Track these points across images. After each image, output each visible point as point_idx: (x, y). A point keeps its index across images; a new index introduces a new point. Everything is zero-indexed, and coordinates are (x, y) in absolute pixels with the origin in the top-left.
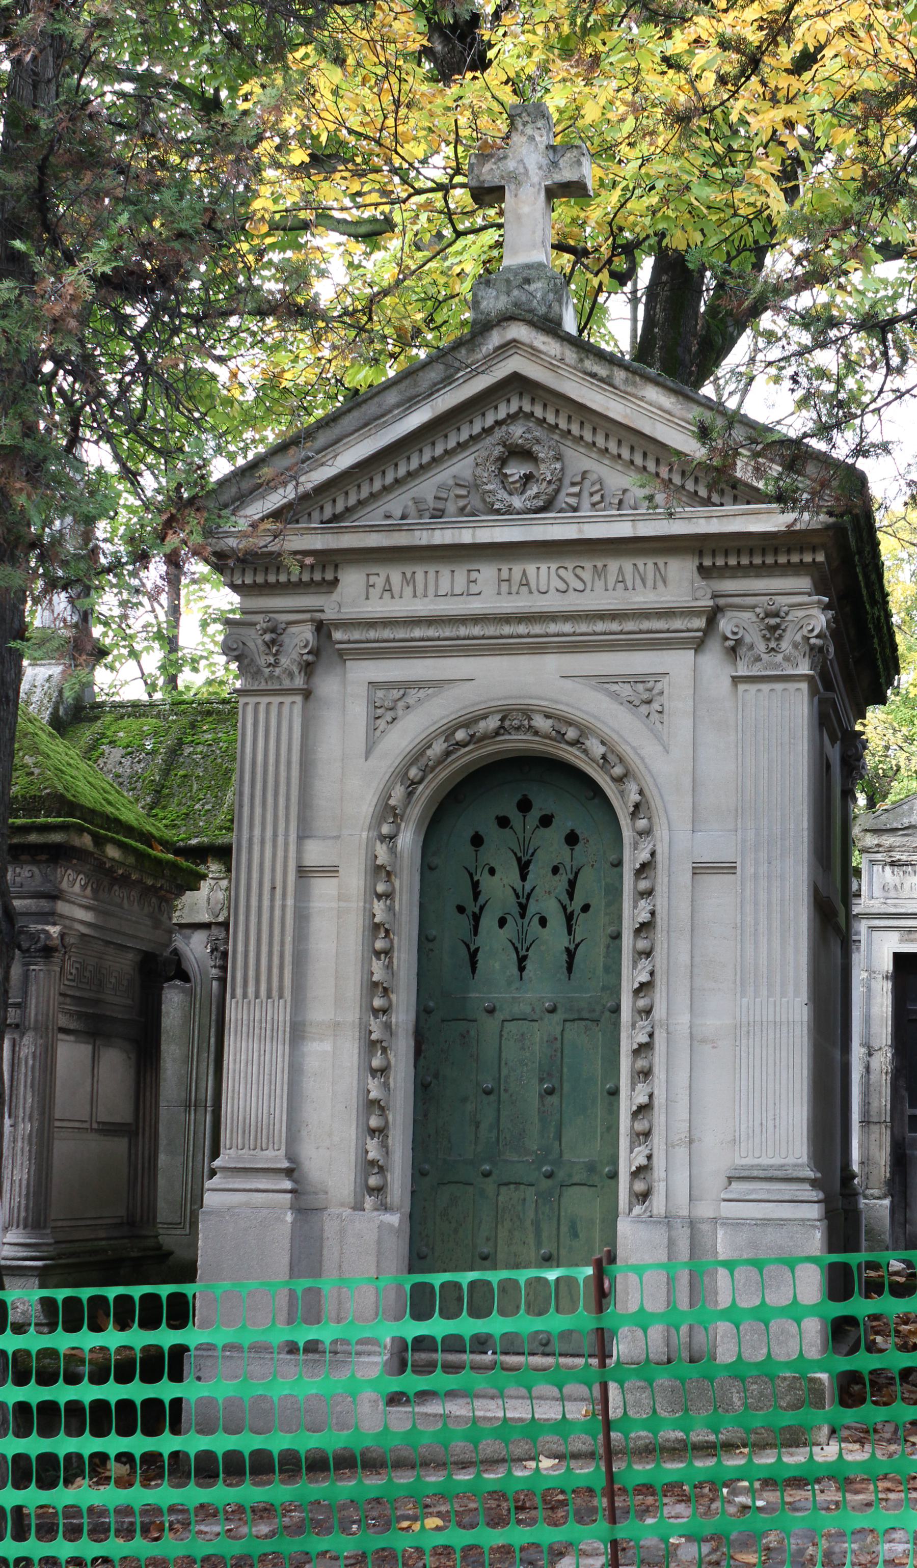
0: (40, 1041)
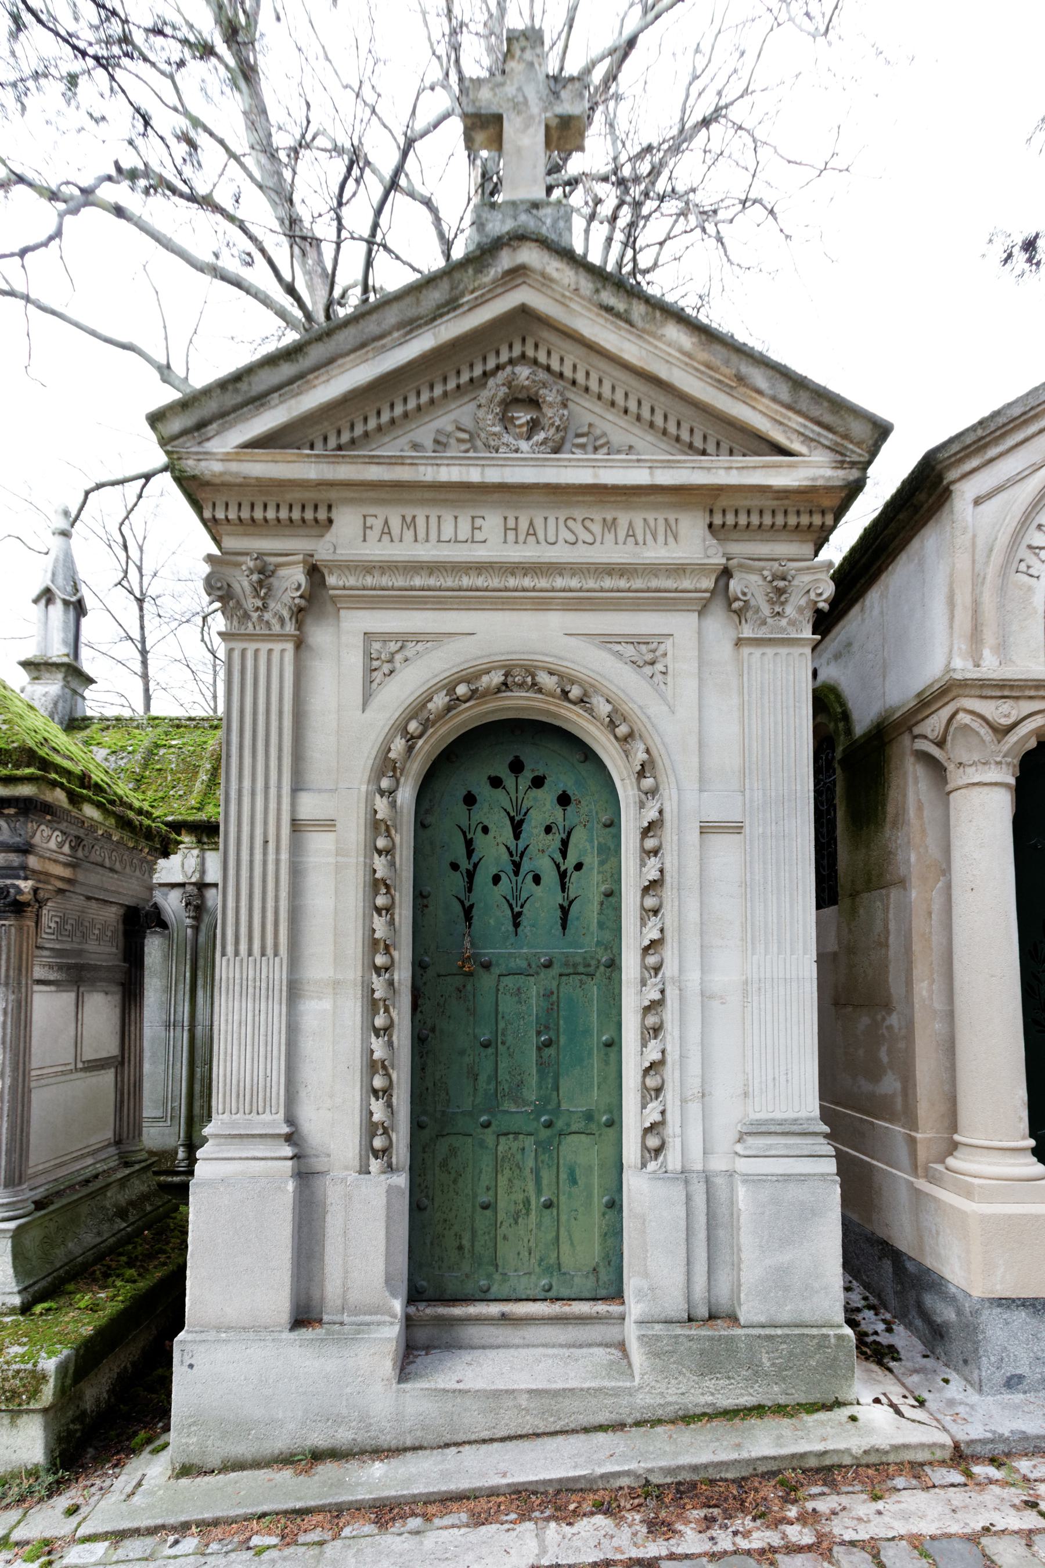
0: (12, 997)
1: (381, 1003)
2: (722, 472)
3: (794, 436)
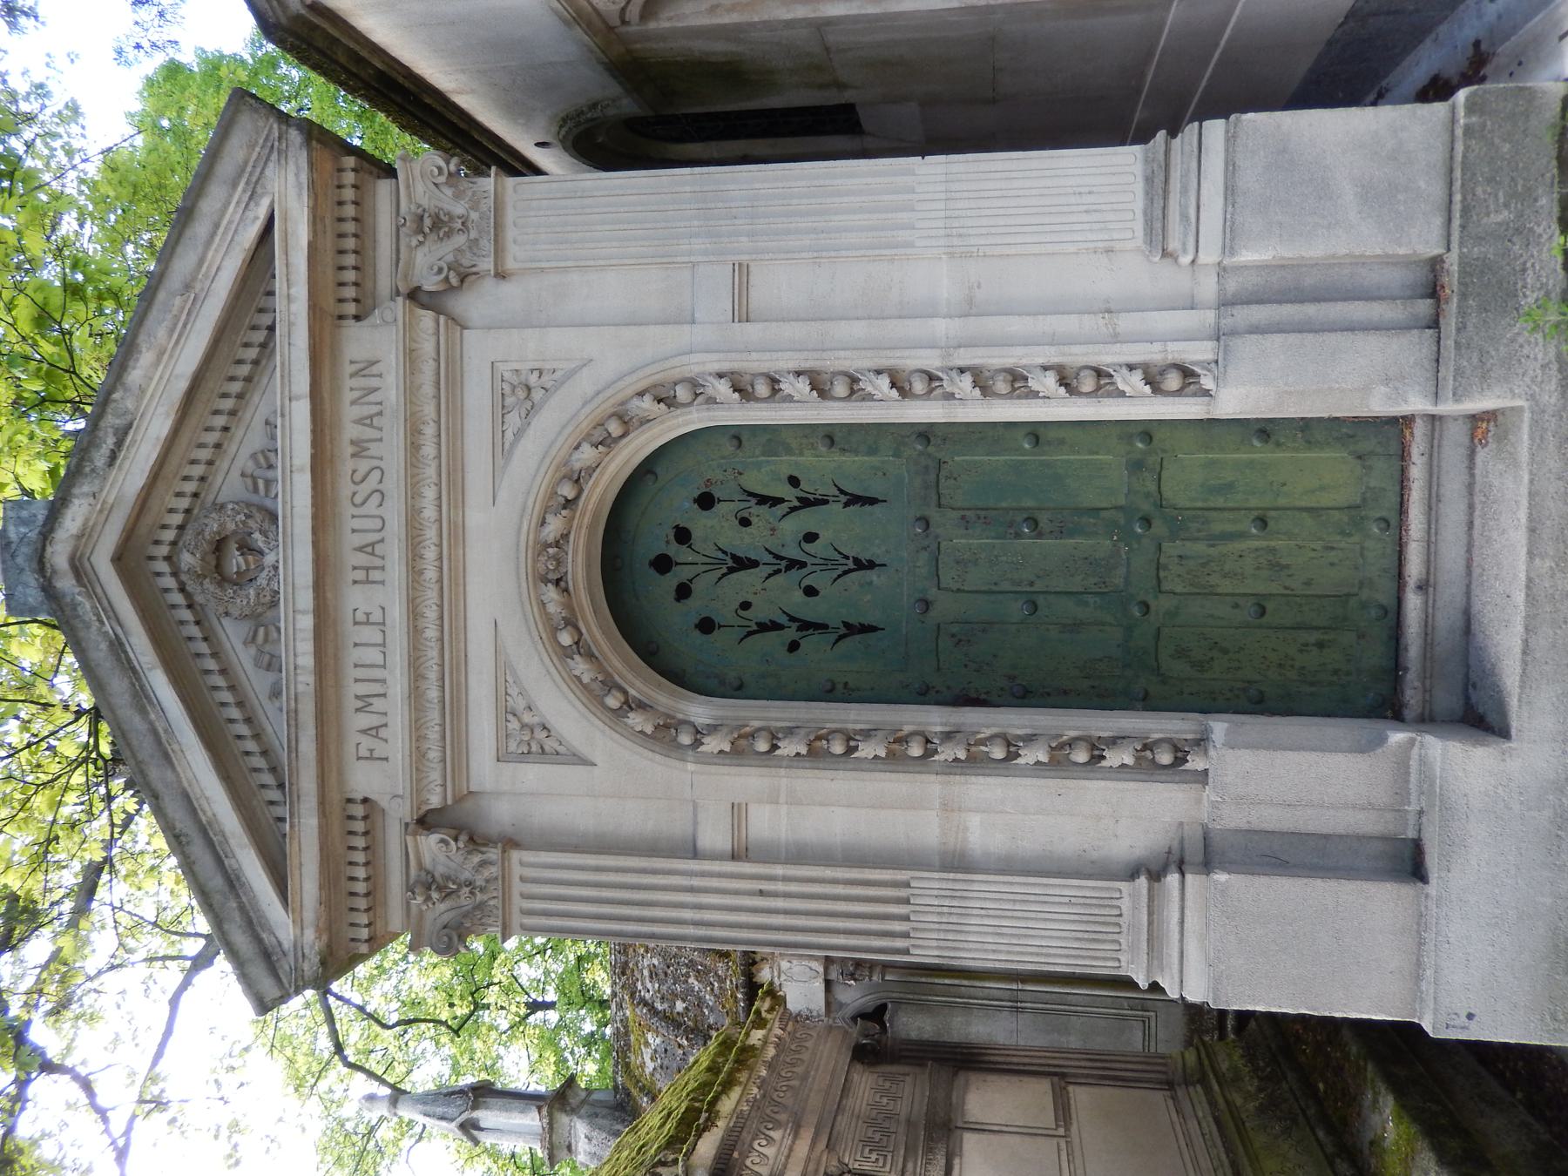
1: (973, 749)
2: (294, 307)
3: (250, 214)
